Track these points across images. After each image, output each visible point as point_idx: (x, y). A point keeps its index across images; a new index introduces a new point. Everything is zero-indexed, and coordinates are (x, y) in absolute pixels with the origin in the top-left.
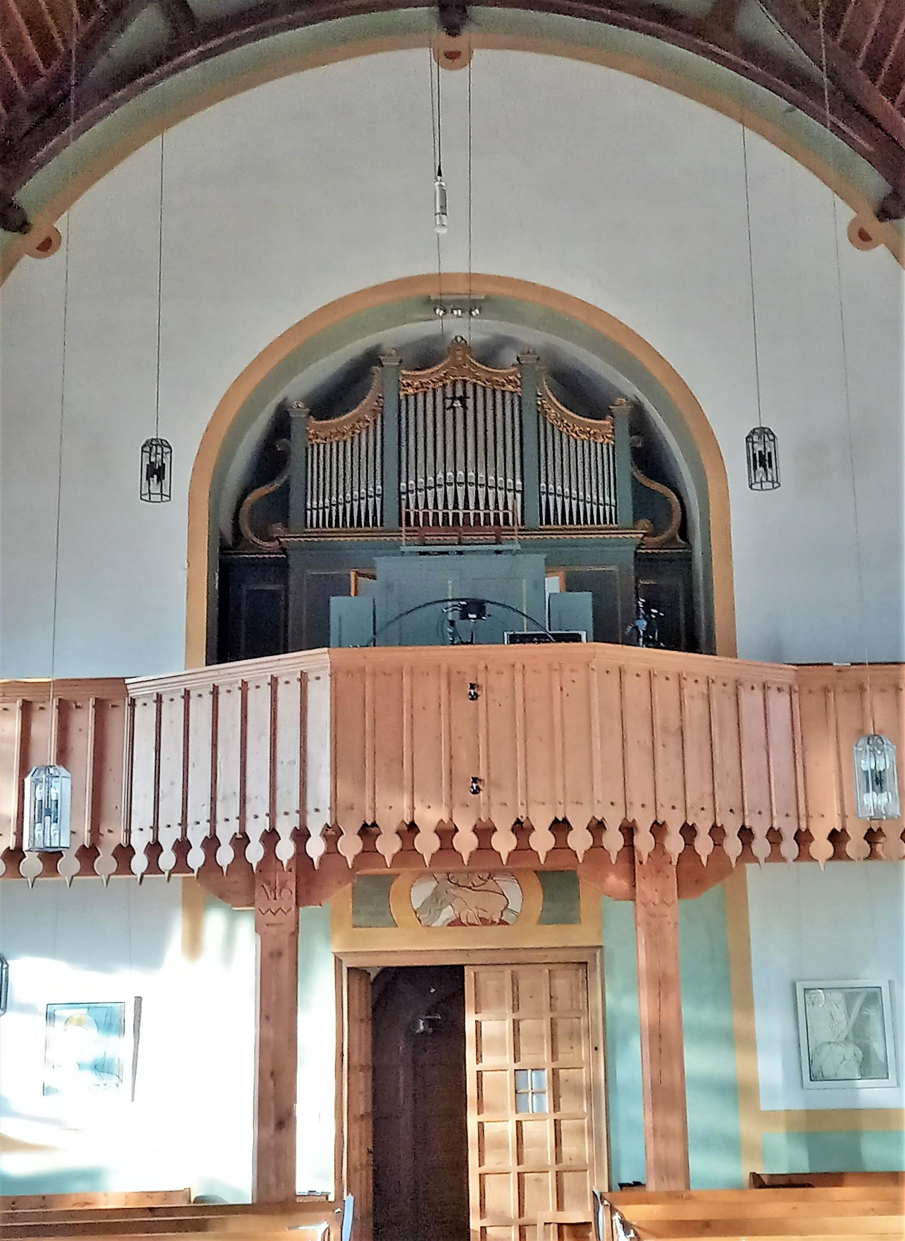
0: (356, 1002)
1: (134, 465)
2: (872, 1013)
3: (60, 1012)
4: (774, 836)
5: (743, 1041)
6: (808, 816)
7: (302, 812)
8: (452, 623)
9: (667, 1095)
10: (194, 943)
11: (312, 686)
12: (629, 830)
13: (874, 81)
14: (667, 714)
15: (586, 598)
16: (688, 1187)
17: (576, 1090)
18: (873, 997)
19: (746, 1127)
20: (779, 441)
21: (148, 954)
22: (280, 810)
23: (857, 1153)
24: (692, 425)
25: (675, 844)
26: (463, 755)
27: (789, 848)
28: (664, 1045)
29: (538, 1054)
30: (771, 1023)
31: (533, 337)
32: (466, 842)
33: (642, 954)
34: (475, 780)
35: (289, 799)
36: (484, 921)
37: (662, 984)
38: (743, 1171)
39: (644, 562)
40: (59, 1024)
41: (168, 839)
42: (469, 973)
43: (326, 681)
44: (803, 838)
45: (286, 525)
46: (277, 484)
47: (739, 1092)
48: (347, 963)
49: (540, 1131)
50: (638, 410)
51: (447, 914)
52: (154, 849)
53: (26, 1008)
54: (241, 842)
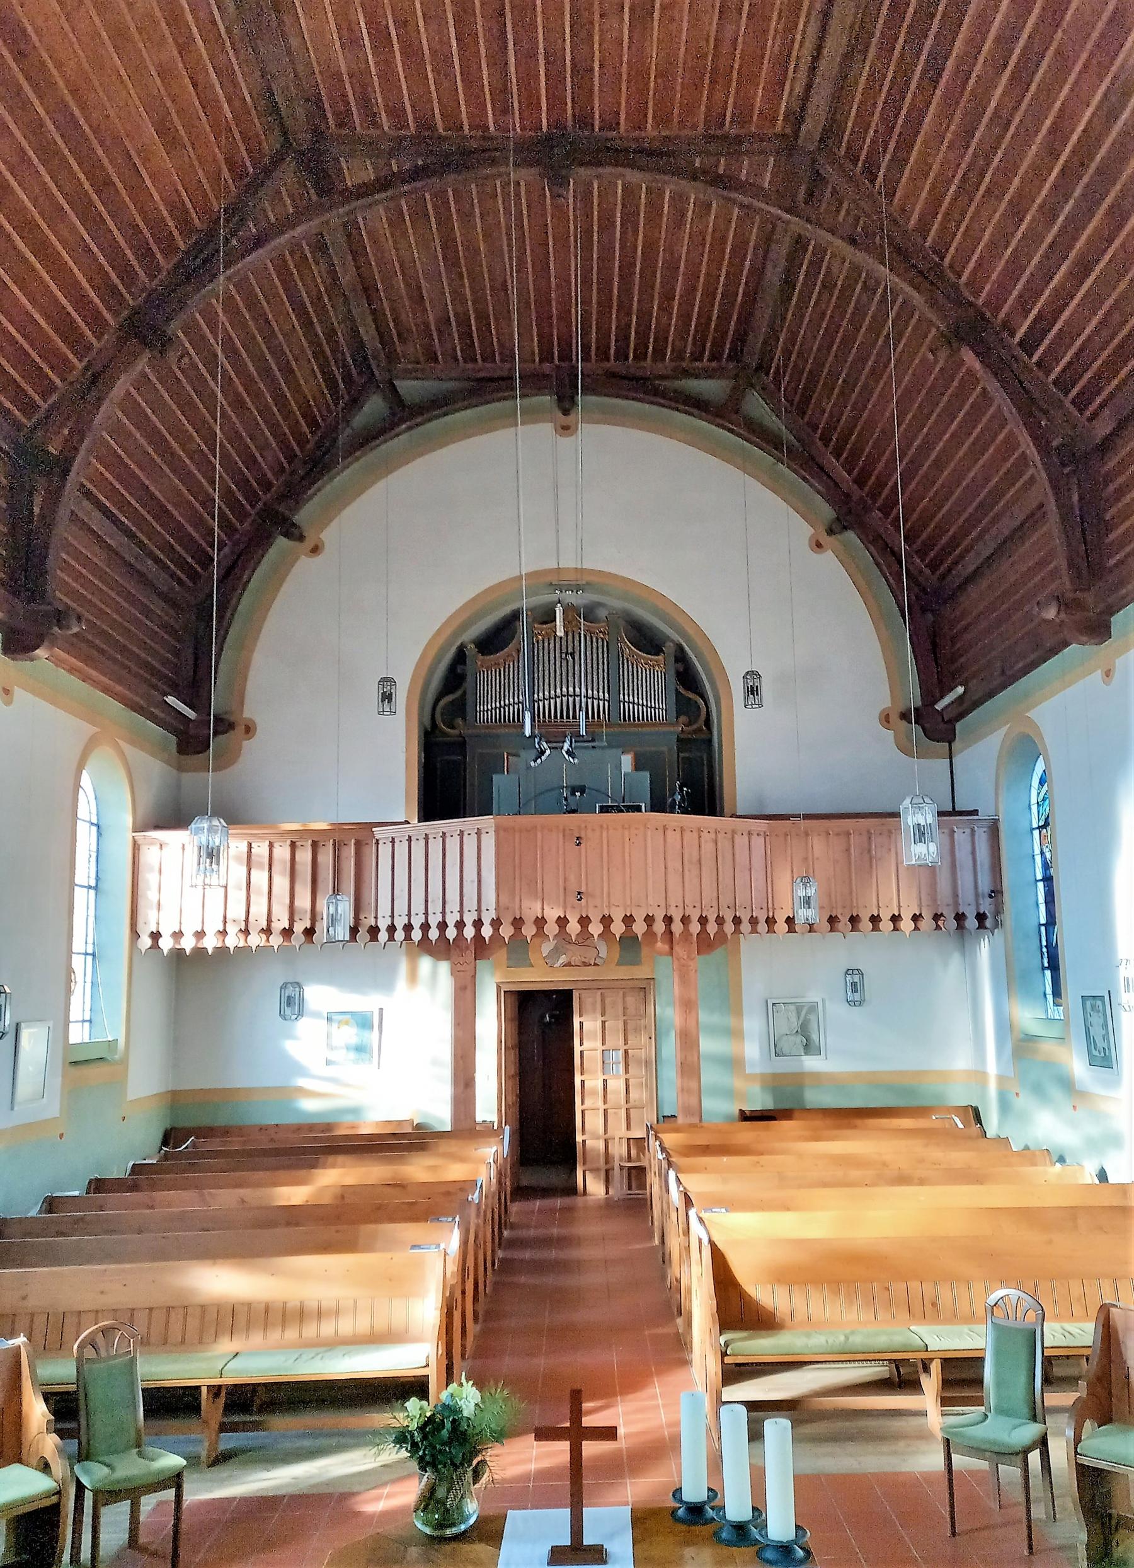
0: (509, 1010)
1: (374, 693)
2: (812, 1017)
3: (335, 1017)
4: (754, 921)
5: (736, 1034)
6: (774, 909)
7: (479, 910)
8: (566, 799)
9: (690, 1069)
10: (413, 977)
11: (484, 837)
12: (668, 920)
13: (827, 446)
14: (691, 853)
15: (646, 776)
16: (701, 1120)
17: (639, 1062)
18: (813, 1008)
19: (738, 1084)
20: (763, 679)
21: (386, 984)
22: (466, 909)
23: (800, 1097)
24: (712, 666)
25: (695, 928)
26: (572, 878)
27: (762, 927)
28: (688, 1040)
29: (616, 1040)
30: (753, 1024)
31: (617, 604)
32: (574, 927)
33: (676, 987)
34: (579, 893)
35: (471, 903)
36: (585, 964)
37: (688, 1005)
38: (734, 1109)
39: (683, 742)
40: (335, 1025)
41: (400, 923)
42: (575, 995)
43: (492, 833)
44: (770, 921)
45: (464, 718)
46: (459, 693)
47: (735, 1064)
48: (504, 988)
49: (617, 1085)
50: (680, 648)
51: (563, 959)
52: (392, 929)
53: (316, 1015)
54: (443, 926)
